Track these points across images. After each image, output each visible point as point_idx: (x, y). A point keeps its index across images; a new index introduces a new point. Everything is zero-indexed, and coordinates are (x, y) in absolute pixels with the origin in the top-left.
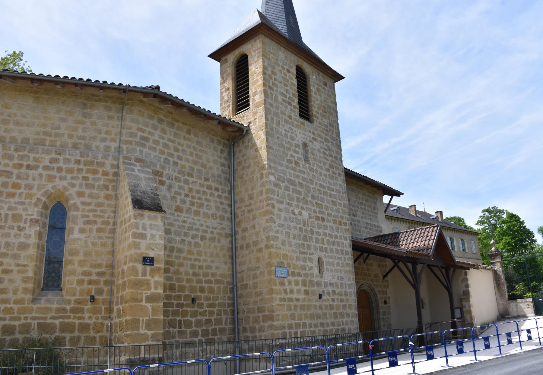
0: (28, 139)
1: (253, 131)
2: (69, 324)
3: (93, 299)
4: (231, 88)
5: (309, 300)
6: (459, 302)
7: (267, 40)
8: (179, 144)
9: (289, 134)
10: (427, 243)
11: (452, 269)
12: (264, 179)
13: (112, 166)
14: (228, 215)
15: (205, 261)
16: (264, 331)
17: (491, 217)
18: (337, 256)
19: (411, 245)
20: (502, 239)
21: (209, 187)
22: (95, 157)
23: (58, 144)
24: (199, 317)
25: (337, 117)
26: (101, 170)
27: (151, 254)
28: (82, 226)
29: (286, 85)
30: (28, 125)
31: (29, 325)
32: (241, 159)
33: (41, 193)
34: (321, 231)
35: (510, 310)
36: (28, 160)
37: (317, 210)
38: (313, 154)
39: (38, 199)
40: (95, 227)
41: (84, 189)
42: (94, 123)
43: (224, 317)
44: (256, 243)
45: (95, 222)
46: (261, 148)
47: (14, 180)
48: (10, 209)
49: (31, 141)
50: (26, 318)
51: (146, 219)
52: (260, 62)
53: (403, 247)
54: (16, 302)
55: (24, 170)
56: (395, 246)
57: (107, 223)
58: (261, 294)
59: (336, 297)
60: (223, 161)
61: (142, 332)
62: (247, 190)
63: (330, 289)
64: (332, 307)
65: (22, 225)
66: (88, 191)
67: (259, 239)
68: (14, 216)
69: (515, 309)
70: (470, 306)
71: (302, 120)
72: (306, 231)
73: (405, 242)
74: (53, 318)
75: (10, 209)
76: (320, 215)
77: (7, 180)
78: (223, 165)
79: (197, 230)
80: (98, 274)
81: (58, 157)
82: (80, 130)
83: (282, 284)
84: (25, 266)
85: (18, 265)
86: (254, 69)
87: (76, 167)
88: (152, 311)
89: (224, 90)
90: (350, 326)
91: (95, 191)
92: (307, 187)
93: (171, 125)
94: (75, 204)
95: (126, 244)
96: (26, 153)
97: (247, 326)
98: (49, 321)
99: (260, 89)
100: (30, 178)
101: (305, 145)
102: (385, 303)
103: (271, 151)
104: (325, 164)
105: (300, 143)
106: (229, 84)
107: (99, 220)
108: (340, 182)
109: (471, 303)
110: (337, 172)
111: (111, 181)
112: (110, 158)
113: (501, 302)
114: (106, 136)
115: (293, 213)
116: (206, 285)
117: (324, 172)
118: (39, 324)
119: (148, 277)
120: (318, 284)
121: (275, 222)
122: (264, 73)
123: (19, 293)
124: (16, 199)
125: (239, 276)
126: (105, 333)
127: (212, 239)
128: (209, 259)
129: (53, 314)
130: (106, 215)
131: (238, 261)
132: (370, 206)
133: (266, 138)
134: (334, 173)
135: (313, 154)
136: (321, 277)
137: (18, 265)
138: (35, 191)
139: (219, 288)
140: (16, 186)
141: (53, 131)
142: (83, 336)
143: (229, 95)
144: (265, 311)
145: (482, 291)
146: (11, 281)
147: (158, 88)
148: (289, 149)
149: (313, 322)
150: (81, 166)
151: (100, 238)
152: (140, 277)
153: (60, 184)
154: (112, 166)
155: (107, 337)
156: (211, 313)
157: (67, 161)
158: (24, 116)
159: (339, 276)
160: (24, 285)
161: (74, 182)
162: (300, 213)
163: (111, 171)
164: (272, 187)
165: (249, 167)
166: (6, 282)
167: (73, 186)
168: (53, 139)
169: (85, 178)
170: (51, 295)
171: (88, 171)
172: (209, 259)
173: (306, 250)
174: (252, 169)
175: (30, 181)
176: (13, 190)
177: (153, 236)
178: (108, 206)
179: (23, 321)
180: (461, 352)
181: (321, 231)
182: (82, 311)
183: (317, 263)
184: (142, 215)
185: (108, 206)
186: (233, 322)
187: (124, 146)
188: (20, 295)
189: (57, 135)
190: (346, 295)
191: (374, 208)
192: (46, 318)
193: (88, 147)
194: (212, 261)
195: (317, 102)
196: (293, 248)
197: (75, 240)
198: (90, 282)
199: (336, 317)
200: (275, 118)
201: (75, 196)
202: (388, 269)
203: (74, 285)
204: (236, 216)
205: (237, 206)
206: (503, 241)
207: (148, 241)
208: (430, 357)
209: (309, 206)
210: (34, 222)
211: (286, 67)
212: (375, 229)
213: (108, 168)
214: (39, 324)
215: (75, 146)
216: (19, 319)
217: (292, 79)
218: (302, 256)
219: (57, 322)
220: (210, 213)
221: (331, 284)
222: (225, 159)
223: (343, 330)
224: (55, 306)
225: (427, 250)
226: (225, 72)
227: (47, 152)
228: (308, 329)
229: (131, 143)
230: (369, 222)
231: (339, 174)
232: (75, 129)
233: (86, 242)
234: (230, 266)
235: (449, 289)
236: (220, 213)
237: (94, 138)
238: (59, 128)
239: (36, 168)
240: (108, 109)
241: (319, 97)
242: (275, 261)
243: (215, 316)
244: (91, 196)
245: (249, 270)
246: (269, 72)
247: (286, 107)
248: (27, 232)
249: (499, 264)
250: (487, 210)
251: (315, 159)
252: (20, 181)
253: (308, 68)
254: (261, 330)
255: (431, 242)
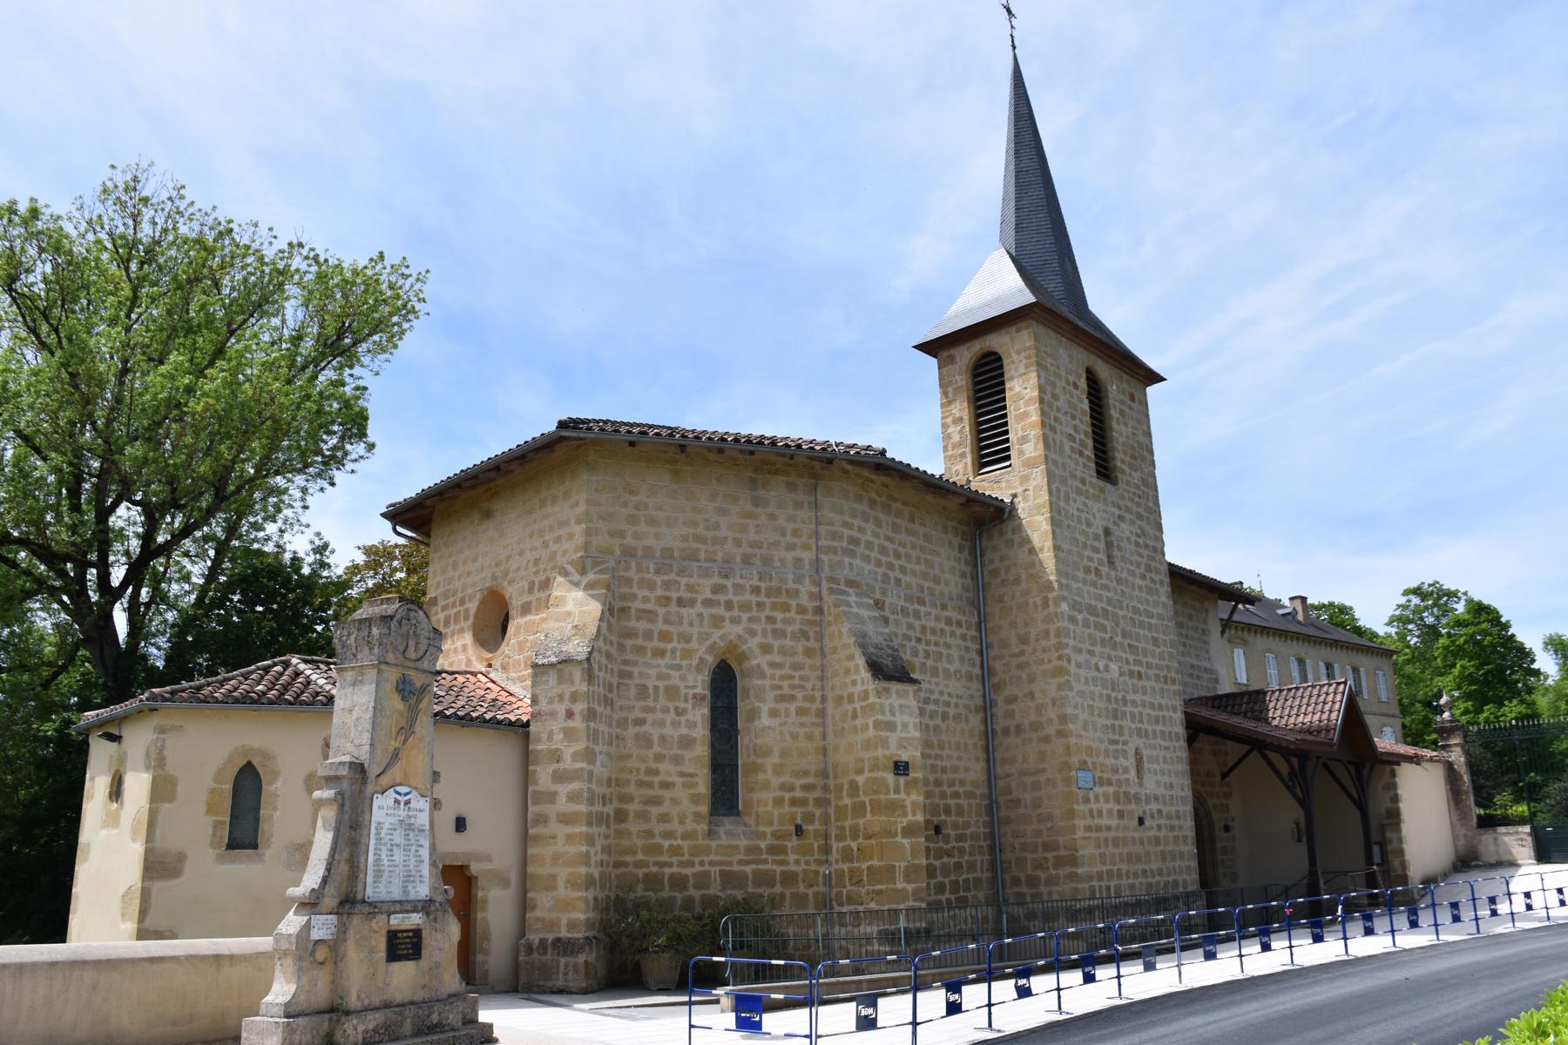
0: (671, 550)
1: (1021, 513)
2: (766, 873)
3: (799, 830)
4: (966, 418)
5: (1126, 828)
6: (1379, 830)
7: (1041, 330)
8: (900, 544)
9: (1084, 515)
10: (1325, 716)
11: (1368, 765)
12: (1052, 609)
13: (812, 596)
14: (977, 671)
15: (949, 757)
16: (1057, 884)
17: (1426, 608)
18: (1164, 744)
19: (1292, 720)
20: (1454, 666)
21: (949, 621)
22: (783, 581)
23: (719, 557)
24: (945, 859)
25: (1153, 464)
26: (793, 603)
27: (904, 756)
28: (773, 705)
29: (1074, 417)
30: (669, 525)
31: (706, 874)
32: (997, 564)
33: (704, 648)
34: (1138, 698)
35: (1482, 848)
36: (678, 590)
37: (1131, 658)
38: (1120, 549)
39: (702, 660)
40: (793, 707)
41: (770, 640)
42: (772, 517)
43: (979, 858)
44: (1036, 726)
45: (792, 698)
46: (1042, 549)
47: (660, 625)
48: (660, 677)
49: (677, 554)
50: (702, 863)
51: (894, 696)
52: (1033, 379)
53: (1275, 723)
54: (685, 836)
55: (673, 608)
56: (1258, 719)
57: (811, 699)
58: (1049, 817)
59: (1163, 822)
60: (963, 567)
61: (899, 886)
62: (1013, 625)
63: (1154, 807)
64: (1157, 841)
65: (681, 705)
66: (776, 644)
67: (1043, 719)
68: (667, 689)
69: (1492, 848)
70: (1400, 840)
71: (1102, 483)
72: (1116, 699)
73: (1278, 713)
74: (741, 862)
75: (660, 677)
76: (1136, 668)
77: (650, 626)
78: (963, 575)
79: (936, 702)
80: (806, 788)
81: (725, 582)
82: (752, 531)
83: (1087, 801)
84: (692, 775)
85: (682, 774)
86: (1018, 389)
87: (754, 599)
88: (909, 851)
89: (949, 420)
90: (1185, 876)
91: (788, 642)
92: (1114, 614)
93: (887, 509)
94: (759, 666)
95: (860, 738)
96: (673, 576)
97: (1022, 876)
98: (736, 868)
99: (1035, 433)
100: (685, 621)
101: (1107, 532)
102: (1227, 829)
103: (1061, 554)
104: (1138, 565)
105: (1100, 532)
106: (961, 409)
107: (800, 695)
108: (1164, 599)
109: (1404, 833)
110: (1157, 578)
111: (813, 623)
112: (807, 581)
113: (1462, 832)
114: (793, 540)
115: (1098, 669)
116: (952, 802)
117: (1138, 582)
118: (722, 873)
119: (903, 796)
120: (1137, 799)
121: (1071, 689)
122: (1041, 401)
123: (688, 820)
124: (668, 660)
125: (1001, 783)
126: (821, 889)
127: (957, 717)
128: (955, 755)
129: (741, 857)
130: (809, 686)
131: (998, 756)
132: (1196, 629)
133: (1054, 532)
134: (1153, 581)
135: (1120, 549)
136: (1141, 785)
137: (682, 774)
138: (694, 645)
139: (970, 805)
140: (665, 637)
141: (709, 534)
142: (788, 892)
143: (962, 432)
144: (1058, 849)
145: (1424, 808)
146: (674, 801)
147: (883, 452)
148: (1085, 545)
149: (1133, 868)
150: (763, 598)
151: (803, 725)
152: (892, 796)
153: (733, 631)
154: (812, 596)
155: (824, 895)
156: (961, 851)
157: (738, 588)
158: (660, 508)
159: (1164, 777)
160: (693, 808)
161: (754, 626)
162: (1107, 668)
163: (810, 605)
164: (1065, 624)
165: (1017, 581)
166: (667, 803)
167: (753, 633)
168: (711, 549)
169: (771, 620)
170: (728, 824)
171: (774, 606)
172: (955, 755)
173: (1116, 737)
174: (1023, 585)
175: (685, 628)
176: (662, 645)
177: (905, 725)
178: (812, 668)
179: (698, 868)
180: (1369, 932)
181: (1138, 698)
182: (783, 850)
183: (1133, 760)
184: (887, 690)
185: (812, 668)
186: (993, 867)
187: (822, 556)
188: (690, 825)
189: (715, 541)
190: (1178, 818)
191: (1204, 632)
192: (731, 864)
193: (767, 561)
194: (959, 758)
195: (1122, 440)
196: (1100, 734)
197: (765, 729)
198: (793, 802)
199: (1164, 859)
200: (1063, 489)
201: (757, 651)
202: (1230, 762)
203: (769, 808)
204: (991, 672)
205: (992, 653)
206: (1456, 671)
207: (899, 734)
208: (1318, 939)
209: (1120, 653)
210: (698, 699)
211: (1071, 379)
212: (1206, 676)
213: (804, 599)
214: (722, 873)
215: (747, 560)
216: (692, 864)
217: (1081, 401)
218: (1112, 747)
219: (748, 869)
220: (952, 669)
221: (1156, 798)
222: (967, 563)
223: (1176, 883)
224: (743, 843)
225: (1328, 731)
226: (950, 384)
227: (706, 573)
228: (1124, 882)
229: (834, 550)
230: (1195, 662)
231: (1162, 582)
232: (743, 529)
233: (781, 733)
234: (983, 764)
235: (1361, 806)
236: (965, 668)
237: (775, 545)
238: (717, 527)
239: (692, 603)
240: (792, 487)
241: (1123, 428)
242: (1075, 760)
243: (967, 857)
244: (783, 651)
245: (1022, 773)
246: (1048, 397)
247: (1077, 462)
248: (690, 717)
249: (1458, 749)
250: (1417, 591)
251: (1123, 559)
252: (670, 628)
253: (1104, 371)
254: (1051, 881)
255: (1334, 716)
